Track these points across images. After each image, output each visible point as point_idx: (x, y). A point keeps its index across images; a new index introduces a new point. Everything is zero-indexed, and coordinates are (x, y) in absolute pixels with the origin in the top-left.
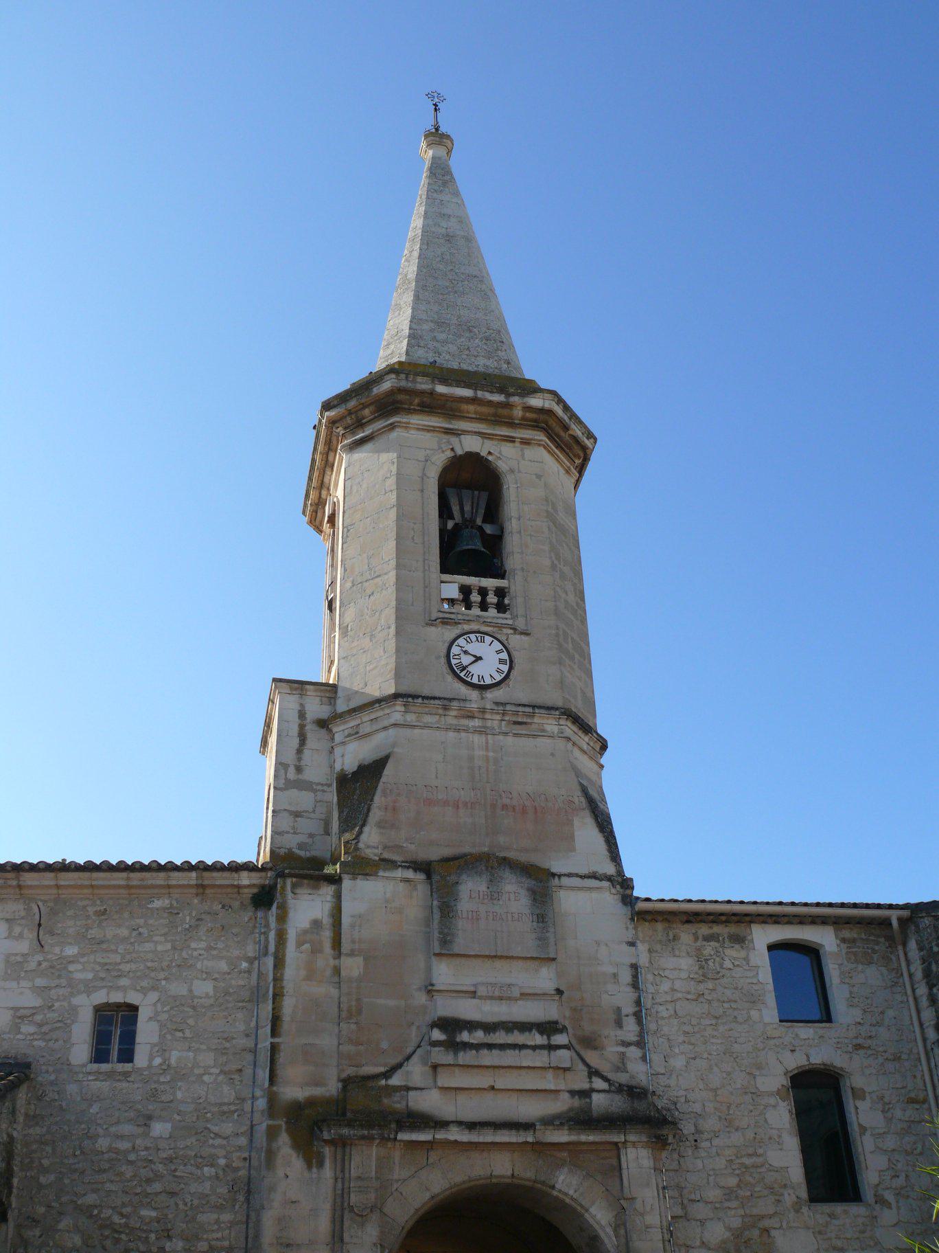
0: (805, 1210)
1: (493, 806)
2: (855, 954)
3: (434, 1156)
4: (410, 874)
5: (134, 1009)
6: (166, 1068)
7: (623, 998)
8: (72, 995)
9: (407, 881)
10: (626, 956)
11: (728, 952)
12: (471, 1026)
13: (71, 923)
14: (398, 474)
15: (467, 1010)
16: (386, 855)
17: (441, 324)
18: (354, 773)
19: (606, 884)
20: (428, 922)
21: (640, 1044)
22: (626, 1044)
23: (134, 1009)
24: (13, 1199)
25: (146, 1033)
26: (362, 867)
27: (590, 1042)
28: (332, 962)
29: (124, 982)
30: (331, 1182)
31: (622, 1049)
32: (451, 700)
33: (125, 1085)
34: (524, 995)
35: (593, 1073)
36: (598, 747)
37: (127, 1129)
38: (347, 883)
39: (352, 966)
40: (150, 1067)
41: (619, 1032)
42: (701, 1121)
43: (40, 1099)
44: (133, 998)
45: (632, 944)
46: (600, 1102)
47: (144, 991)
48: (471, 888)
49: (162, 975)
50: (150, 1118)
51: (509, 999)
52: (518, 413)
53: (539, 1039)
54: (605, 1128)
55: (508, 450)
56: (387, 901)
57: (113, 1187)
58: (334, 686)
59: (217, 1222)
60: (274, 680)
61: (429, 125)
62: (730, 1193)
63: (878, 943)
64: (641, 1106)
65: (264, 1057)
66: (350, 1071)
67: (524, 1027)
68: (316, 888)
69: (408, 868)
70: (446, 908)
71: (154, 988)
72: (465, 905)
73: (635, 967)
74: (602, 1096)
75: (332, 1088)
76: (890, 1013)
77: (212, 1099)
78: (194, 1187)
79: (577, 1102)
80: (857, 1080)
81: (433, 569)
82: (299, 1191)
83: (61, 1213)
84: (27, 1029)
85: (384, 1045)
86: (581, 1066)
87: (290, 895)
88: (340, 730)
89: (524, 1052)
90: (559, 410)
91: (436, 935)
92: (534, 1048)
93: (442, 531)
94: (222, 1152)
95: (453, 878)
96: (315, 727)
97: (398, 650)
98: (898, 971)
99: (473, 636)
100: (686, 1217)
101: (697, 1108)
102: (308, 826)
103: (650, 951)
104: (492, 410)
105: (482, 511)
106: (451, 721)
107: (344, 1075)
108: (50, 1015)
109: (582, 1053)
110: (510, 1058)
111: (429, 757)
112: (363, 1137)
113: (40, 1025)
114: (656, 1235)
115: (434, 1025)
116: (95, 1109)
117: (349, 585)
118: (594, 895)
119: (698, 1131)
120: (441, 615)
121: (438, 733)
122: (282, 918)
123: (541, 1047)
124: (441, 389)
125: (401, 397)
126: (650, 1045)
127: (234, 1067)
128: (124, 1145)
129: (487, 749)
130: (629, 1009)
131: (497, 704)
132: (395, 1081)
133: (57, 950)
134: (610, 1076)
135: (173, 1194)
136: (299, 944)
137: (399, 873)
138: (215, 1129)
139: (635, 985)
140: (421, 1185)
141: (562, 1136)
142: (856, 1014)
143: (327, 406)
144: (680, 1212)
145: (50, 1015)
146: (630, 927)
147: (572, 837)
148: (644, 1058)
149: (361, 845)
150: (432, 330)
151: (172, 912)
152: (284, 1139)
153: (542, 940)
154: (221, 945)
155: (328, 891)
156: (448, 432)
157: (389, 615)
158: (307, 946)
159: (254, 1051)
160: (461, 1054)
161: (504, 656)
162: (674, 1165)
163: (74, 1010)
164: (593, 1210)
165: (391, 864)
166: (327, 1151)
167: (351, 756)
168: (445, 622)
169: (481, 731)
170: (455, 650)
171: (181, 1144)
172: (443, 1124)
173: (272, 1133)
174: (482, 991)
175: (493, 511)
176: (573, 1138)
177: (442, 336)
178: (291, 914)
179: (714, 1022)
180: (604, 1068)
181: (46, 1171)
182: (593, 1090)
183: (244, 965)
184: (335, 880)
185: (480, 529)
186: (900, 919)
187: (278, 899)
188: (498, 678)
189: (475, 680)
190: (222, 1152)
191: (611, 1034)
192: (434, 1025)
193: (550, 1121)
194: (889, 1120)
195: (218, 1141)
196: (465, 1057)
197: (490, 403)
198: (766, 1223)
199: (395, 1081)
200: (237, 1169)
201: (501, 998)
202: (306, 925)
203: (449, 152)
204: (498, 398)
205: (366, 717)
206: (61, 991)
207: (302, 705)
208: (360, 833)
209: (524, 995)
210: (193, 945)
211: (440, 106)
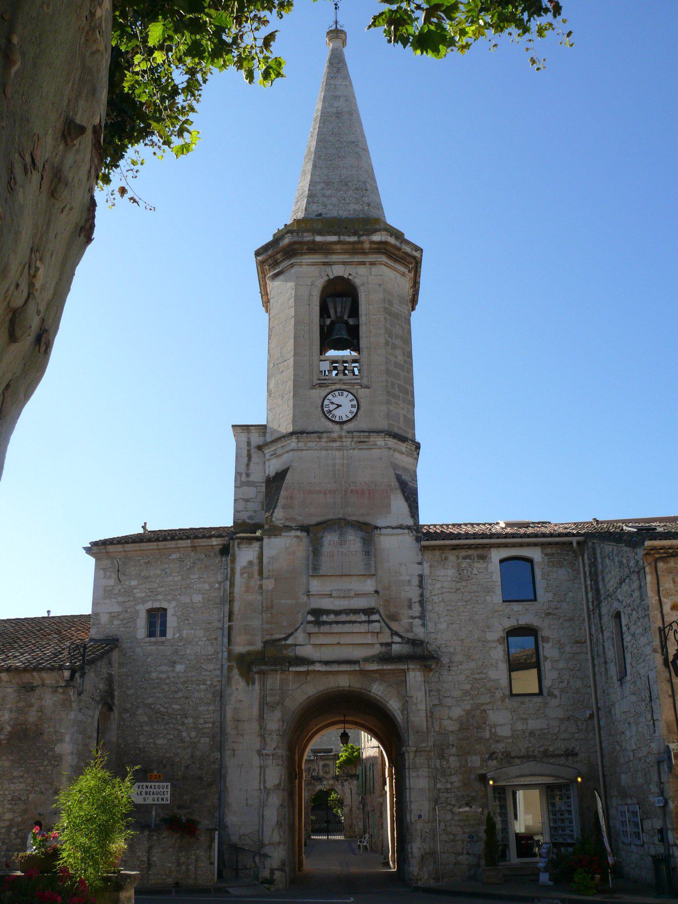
0: (507, 700)
1: (346, 491)
2: (552, 562)
3: (309, 678)
4: (299, 533)
5: (165, 610)
6: (181, 639)
7: (413, 593)
8: (136, 605)
9: (297, 537)
10: (416, 570)
11: (476, 565)
12: (328, 612)
13: (133, 569)
14: (296, 296)
15: (326, 604)
17: (328, 183)
18: (274, 477)
19: (406, 531)
20: (308, 558)
21: (422, 617)
23: (165, 610)
26: (275, 531)
27: (394, 617)
28: (259, 582)
29: (160, 597)
30: (258, 691)
31: (411, 620)
32: (322, 433)
33: (162, 647)
34: (357, 595)
35: (394, 633)
36: (414, 448)
37: (165, 668)
38: (266, 540)
39: (269, 584)
40: (173, 638)
41: (410, 612)
43: (124, 655)
44: (164, 605)
45: (420, 564)
47: (169, 601)
48: (330, 539)
49: (177, 593)
50: (175, 663)
52: (367, 246)
53: (363, 618)
54: (397, 662)
55: (362, 270)
56: (287, 548)
58: (265, 426)
59: (208, 710)
60: (233, 426)
61: (329, 24)
62: (466, 693)
63: (568, 555)
64: (419, 650)
65: (226, 632)
66: (268, 637)
67: (356, 612)
68: (250, 544)
69: (297, 530)
70: (316, 550)
71: (174, 599)
73: (421, 576)
75: (259, 646)
76: (570, 594)
77: (203, 653)
78: (196, 695)
79: (384, 649)
80: (545, 633)
81: (315, 354)
82: (243, 696)
83: (138, 707)
84: (116, 622)
85: (285, 624)
86: (387, 630)
87: (237, 549)
88: (268, 451)
89: (356, 624)
90: (392, 240)
91: (311, 566)
92: (360, 622)
93: (322, 327)
94: (208, 678)
95: (321, 534)
96: (256, 450)
97: (294, 406)
98: (578, 570)
99: (336, 393)
100: (441, 704)
101: (452, 650)
102: (252, 506)
103: (431, 567)
104: (351, 247)
105: (347, 310)
106: (323, 444)
107: (264, 640)
109: (389, 623)
110: (347, 628)
111: (310, 465)
112: (273, 670)
113: (122, 620)
114: (423, 714)
115: (309, 613)
117: (272, 365)
118: (400, 538)
119: (451, 662)
120: (319, 382)
121: (316, 452)
122: (233, 561)
123: (364, 622)
124: (319, 239)
125: (296, 246)
126: (427, 618)
128: (164, 676)
129: (343, 459)
130: (416, 599)
131: (348, 432)
132: (290, 641)
133: (127, 583)
134: (403, 635)
135: (187, 698)
136: (242, 574)
137: (293, 533)
139: (421, 586)
141: (374, 667)
142: (550, 596)
143: (258, 253)
144: (436, 702)
147: (390, 506)
148: (424, 625)
149: (273, 519)
150: (322, 189)
151: (181, 560)
152: (235, 672)
153: (368, 565)
154: (205, 576)
155: (256, 545)
156: (325, 264)
157: (290, 385)
159: (222, 629)
160: (322, 627)
161: (355, 402)
162: (436, 679)
164: (391, 702)
165: (288, 528)
166: (256, 676)
167: (273, 467)
168: (321, 386)
169: (339, 449)
170: (326, 402)
171: (190, 675)
172: (312, 662)
173: (230, 669)
174: (334, 594)
175: (355, 311)
176: (380, 667)
177: (328, 193)
178: (238, 559)
180: (401, 630)
181: (130, 688)
182: (393, 643)
183: (217, 585)
184: (260, 539)
185: (347, 323)
186: (578, 543)
187: (231, 551)
188: (350, 416)
189: (337, 419)
190: (208, 678)
191: (405, 613)
192: (309, 613)
193: (367, 660)
194: (562, 653)
195: (207, 673)
196: (324, 629)
197: (349, 243)
198: (484, 707)
199: (290, 641)
200: (215, 686)
202: (245, 564)
203: (344, 43)
204: (353, 239)
205: (279, 445)
207: (249, 438)
208: (273, 512)
210: (192, 577)
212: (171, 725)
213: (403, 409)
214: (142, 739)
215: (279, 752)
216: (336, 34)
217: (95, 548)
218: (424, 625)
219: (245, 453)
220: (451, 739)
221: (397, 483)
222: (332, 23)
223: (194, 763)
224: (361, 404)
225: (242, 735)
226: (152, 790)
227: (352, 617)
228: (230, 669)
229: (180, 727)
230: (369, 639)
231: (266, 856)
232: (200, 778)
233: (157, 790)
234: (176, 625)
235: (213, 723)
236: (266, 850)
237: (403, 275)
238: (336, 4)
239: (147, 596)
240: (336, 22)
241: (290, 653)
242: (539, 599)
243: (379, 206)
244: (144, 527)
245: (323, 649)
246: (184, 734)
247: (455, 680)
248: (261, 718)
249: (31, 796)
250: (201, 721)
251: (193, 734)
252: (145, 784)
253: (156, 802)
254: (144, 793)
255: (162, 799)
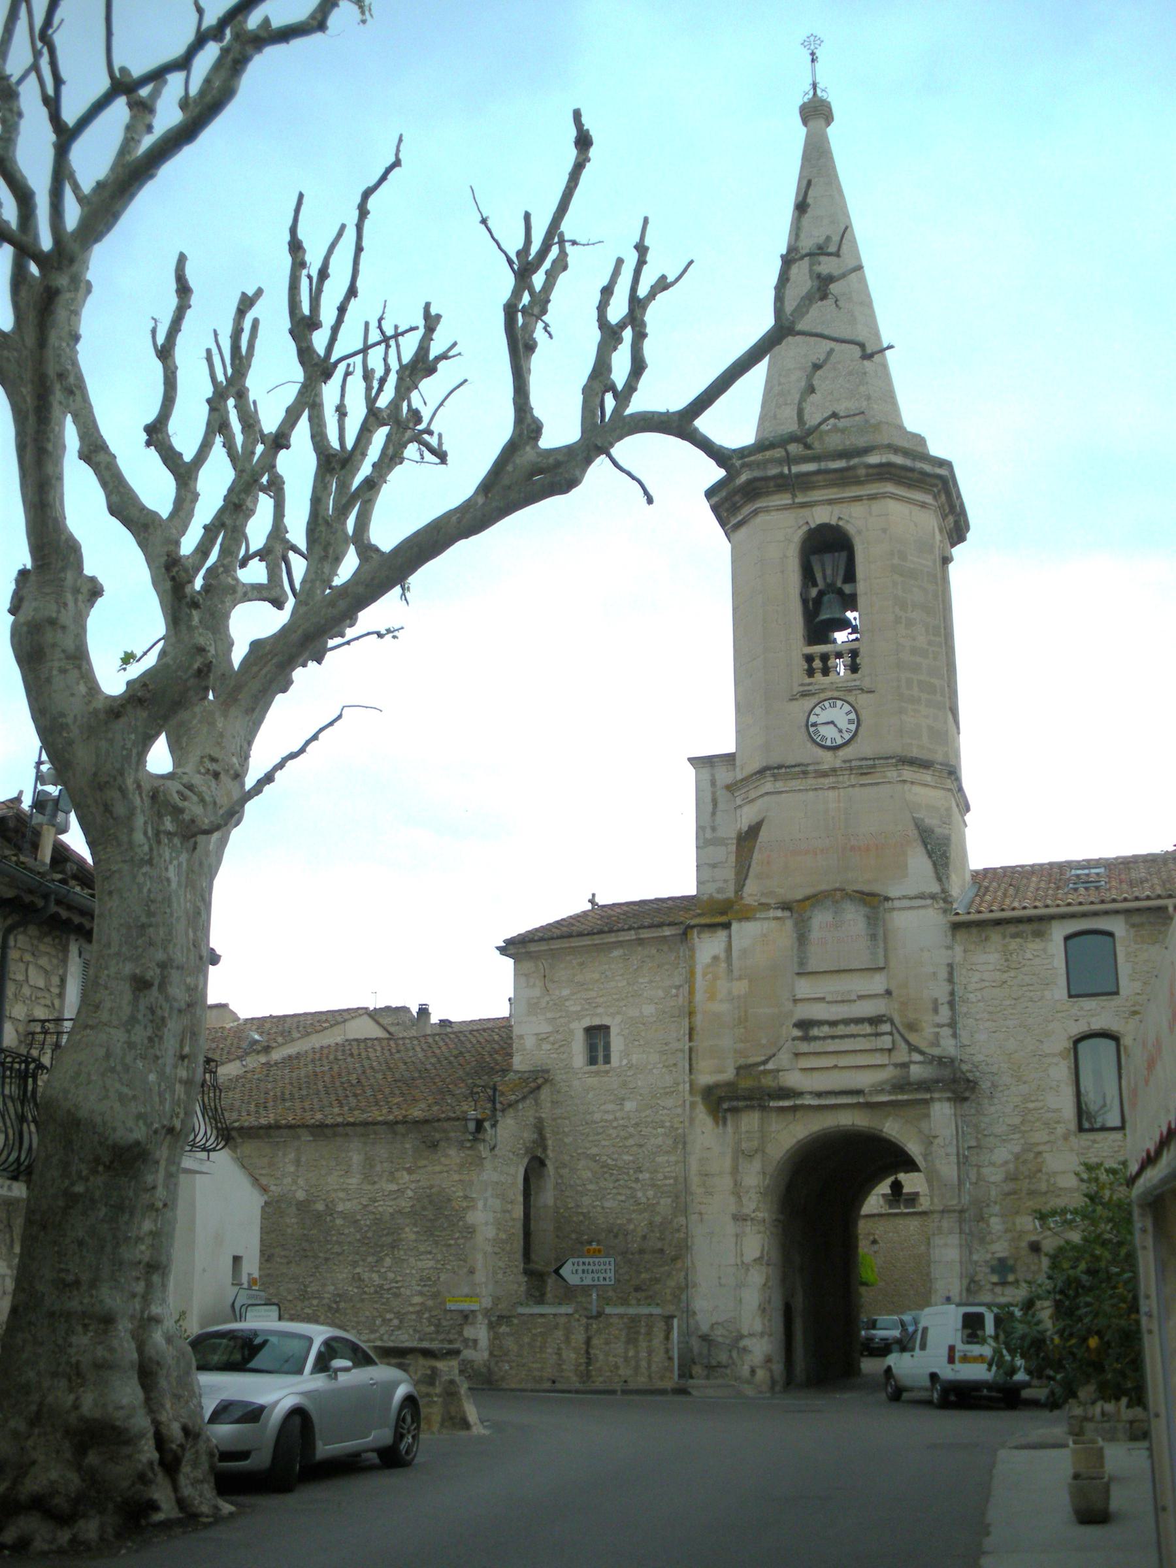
0: (1073, 1139)
3: (799, 1115)
4: (779, 913)
5: (607, 1028)
6: (630, 1066)
7: (941, 991)
8: (569, 1022)
11: (1031, 946)
16: (763, 900)
18: (747, 832)
19: (929, 902)
21: (952, 1024)
22: (939, 1026)
23: (607, 1028)
24: (550, 1153)
25: (617, 1043)
26: (747, 915)
29: (600, 1010)
31: (937, 1030)
33: (606, 1079)
34: (860, 997)
35: (913, 1048)
37: (610, 1107)
38: (735, 926)
40: (620, 1066)
42: (996, 1078)
44: (606, 1021)
45: (949, 948)
46: (917, 1072)
47: (613, 1015)
48: (820, 919)
49: (622, 1004)
50: (623, 1099)
51: (849, 1001)
53: (867, 1029)
56: (765, 935)
57: (606, 1143)
59: (668, 1162)
61: (799, 95)
62: (1015, 1129)
66: (742, 1061)
67: (858, 1021)
69: (777, 908)
71: (618, 1013)
72: (815, 934)
73: (951, 966)
74: (917, 1066)
85: (764, 1041)
86: (903, 1046)
87: (697, 940)
90: (899, 460)
92: (864, 1036)
93: (804, 601)
96: (724, 792)
99: (827, 704)
101: (994, 1069)
103: (965, 951)
105: (841, 572)
107: (738, 1064)
108: (559, 1037)
110: (848, 1045)
112: (747, 1107)
116: (590, 1096)
118: (922, 912)
120: (802, 689)
125: (758, 484)
126: (959, 1026)
127: (671, 1062)
129: (839, 802)
130: (944, 998)
133: (557, 992)
134: (927, 1050)
135: (641, 1146)
136: (704, 975)
137: (771, 913)
138: (662, 1104)
139: (950, 980)
140: (789, 1134)
142: (1137, 986)
145: (559, 1037)
146: (949, 934)
148: (954, 1035)
154: (658, 979)
155: (722, 935)
156: (803, 505)
158: (710, 976)
161: (853, 716)
163: (571, 1032)
165: (765, 906)
167: (747, 817)
168: (805, 695)
171: (643, 1115)
173: (693, 1105)
175: (850, 576)
178: (697, 955)
179: (1013, 1002)
180: (923, 1046)
182: (911, 1062)
183: (674, 991)
189: (829, 743)
196: (816, 1046)
197: (836, 471)
198: (1041, 1148)
200: (677, 1129)
201: (843, 1001)
206: (562, 1020)
207: (713, 775)
209: (860, 997)
210: (641, 980)
211: (818, 53)
212: (621, 1182)
213: (927, 717)
214: (586, 1201)
215: (760, 1215)
216: (816, 112)
217: (511, 947)
218: (954, 1035)
219: (709, 799)
220: (993, 1193)
221: (916, 832)
222: (808, 87)
223: (653, 1231)
224: (862, 718)
225: (711, 1194)
226: (590, 1268)
227: (853, 1029)
228: (693, 1105)
229: (633, 1185)
230: (879, 1059)
231: (745, 1350)
232: (662, 1251)
233: (597, 1267)
234: (622, 1048)
235: (676, 1179)
236: (744, 1342)
237: (923, 505)
238: (813, 54)
239: (583, 1009)
240: (814, 86)
241: (767, 1082)
242: (1122, 992)
243: (889, 397)
244: (592, 901)
245: (816, 1074)
246: (640, 1194)
247: (1000, 1112)
248: (735, 1171)
249: (443, 1277)
250: (660, 1176)
251: (650, 1193)
252: (581, 1260)
253: (596, 1283)
254: (580, 1271)
255: (605, 1279)
